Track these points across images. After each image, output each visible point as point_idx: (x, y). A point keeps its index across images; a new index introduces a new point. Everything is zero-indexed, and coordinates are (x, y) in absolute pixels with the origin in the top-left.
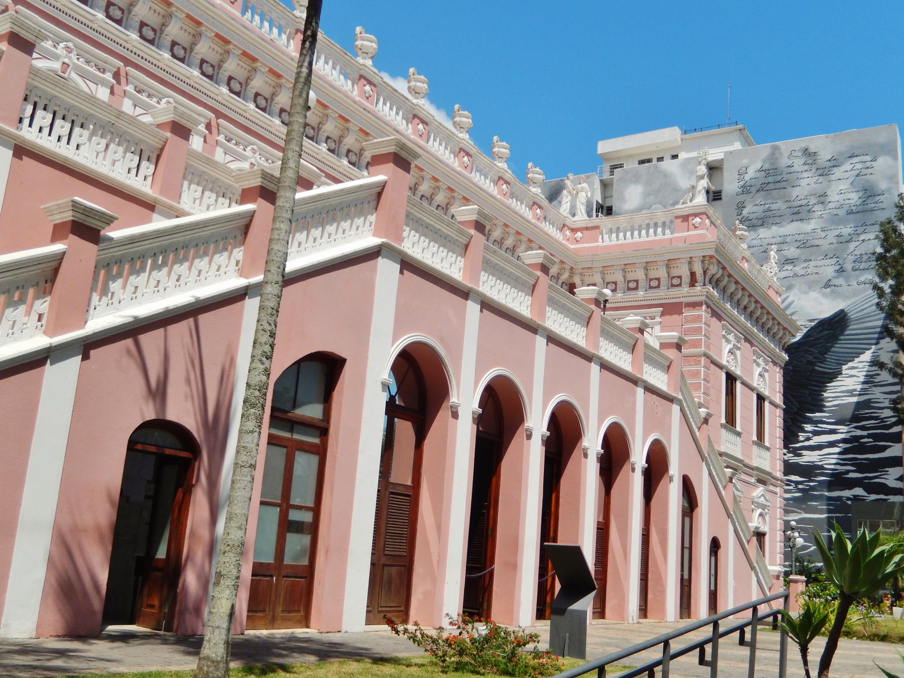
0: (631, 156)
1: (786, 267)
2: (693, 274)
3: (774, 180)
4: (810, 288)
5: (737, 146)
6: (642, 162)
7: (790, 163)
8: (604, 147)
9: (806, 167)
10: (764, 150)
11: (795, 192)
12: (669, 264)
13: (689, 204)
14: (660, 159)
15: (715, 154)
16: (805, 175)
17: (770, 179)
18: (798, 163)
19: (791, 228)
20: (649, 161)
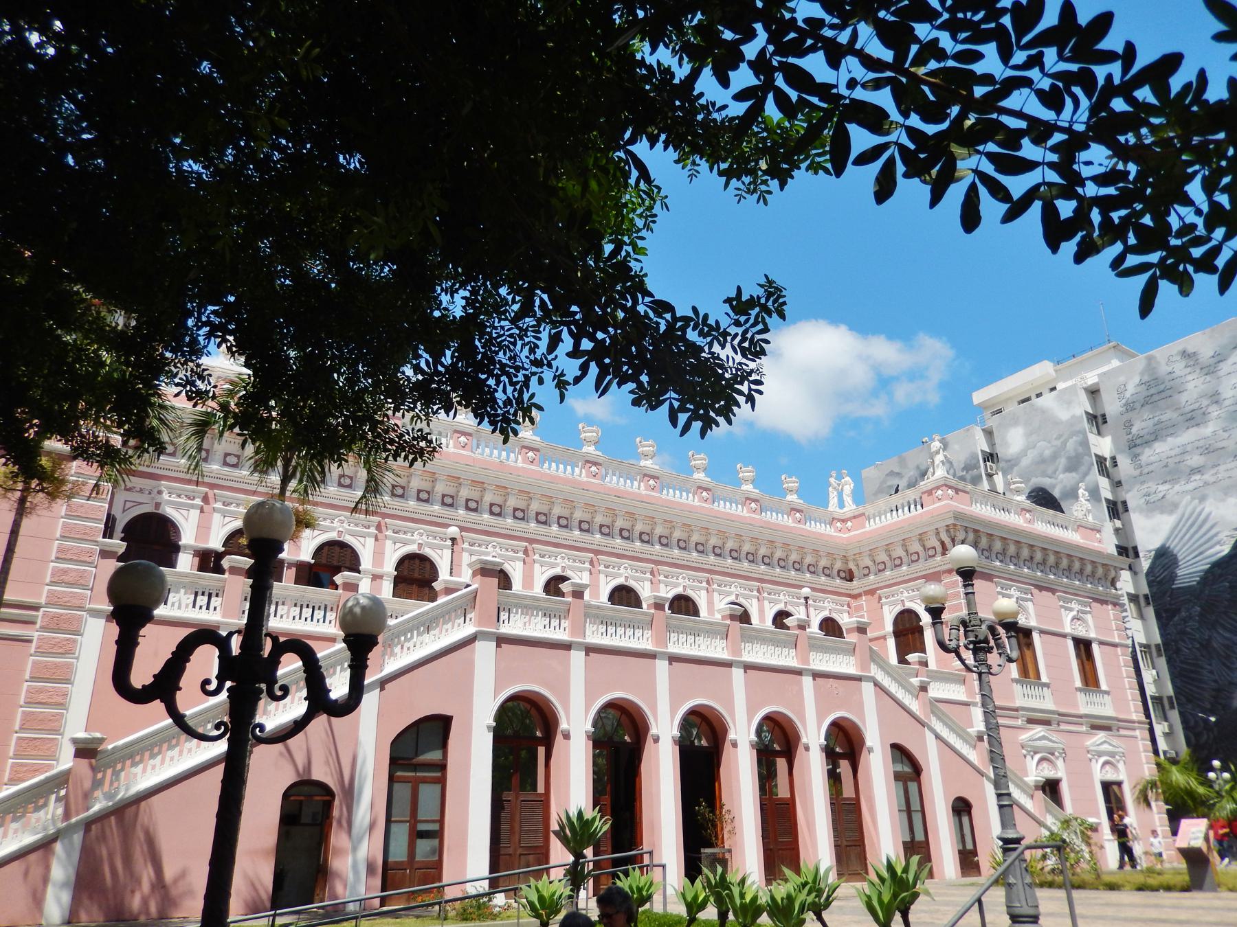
0: (1010, 399)
1: (1194, 478)
2: (943, 543)
3: (1157, 391)
4: (1226, 494)
5: (1115, 363)
6: (1024, 401)
7: (1169, 369)
8: (978, 397)
9: (1189, 370)
10: (1140, 362)
11: (1184, 398)
12: (921, 538)
13: (932, 479)
14: (1039, 395)
15: (1091, 379)
16: (1190, 377)
17: (1153, 391)
18: (1179, 367)
19: (1188, 437)
20: (1028, 399)
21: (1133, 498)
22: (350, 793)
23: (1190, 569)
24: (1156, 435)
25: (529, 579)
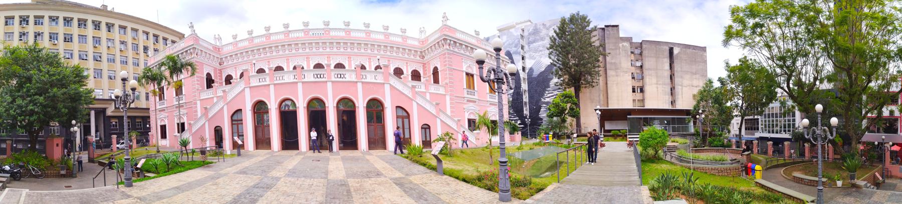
19: (540, 43)
21: (526, 55)
22: (129, 129)
23: (536, 73)
24: (534, 42)
25: (371, 66)
